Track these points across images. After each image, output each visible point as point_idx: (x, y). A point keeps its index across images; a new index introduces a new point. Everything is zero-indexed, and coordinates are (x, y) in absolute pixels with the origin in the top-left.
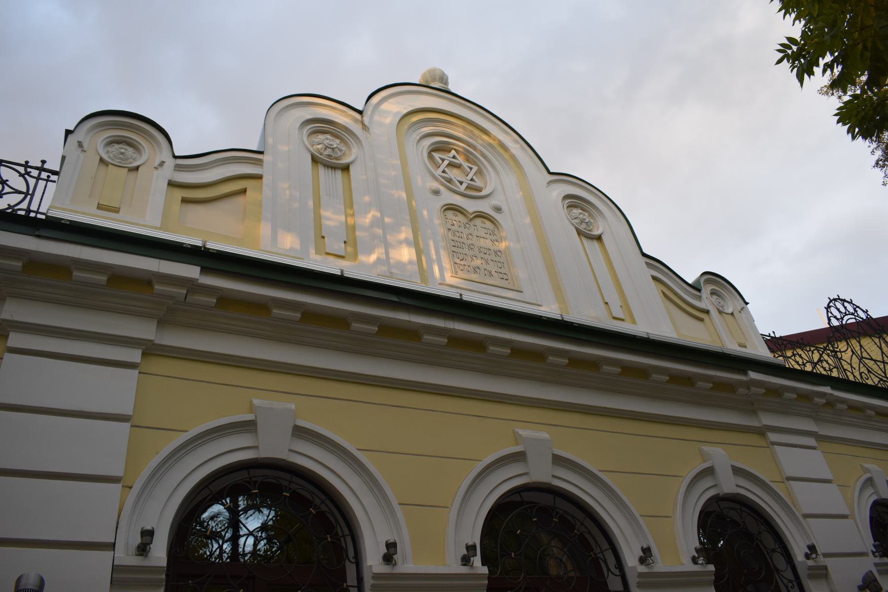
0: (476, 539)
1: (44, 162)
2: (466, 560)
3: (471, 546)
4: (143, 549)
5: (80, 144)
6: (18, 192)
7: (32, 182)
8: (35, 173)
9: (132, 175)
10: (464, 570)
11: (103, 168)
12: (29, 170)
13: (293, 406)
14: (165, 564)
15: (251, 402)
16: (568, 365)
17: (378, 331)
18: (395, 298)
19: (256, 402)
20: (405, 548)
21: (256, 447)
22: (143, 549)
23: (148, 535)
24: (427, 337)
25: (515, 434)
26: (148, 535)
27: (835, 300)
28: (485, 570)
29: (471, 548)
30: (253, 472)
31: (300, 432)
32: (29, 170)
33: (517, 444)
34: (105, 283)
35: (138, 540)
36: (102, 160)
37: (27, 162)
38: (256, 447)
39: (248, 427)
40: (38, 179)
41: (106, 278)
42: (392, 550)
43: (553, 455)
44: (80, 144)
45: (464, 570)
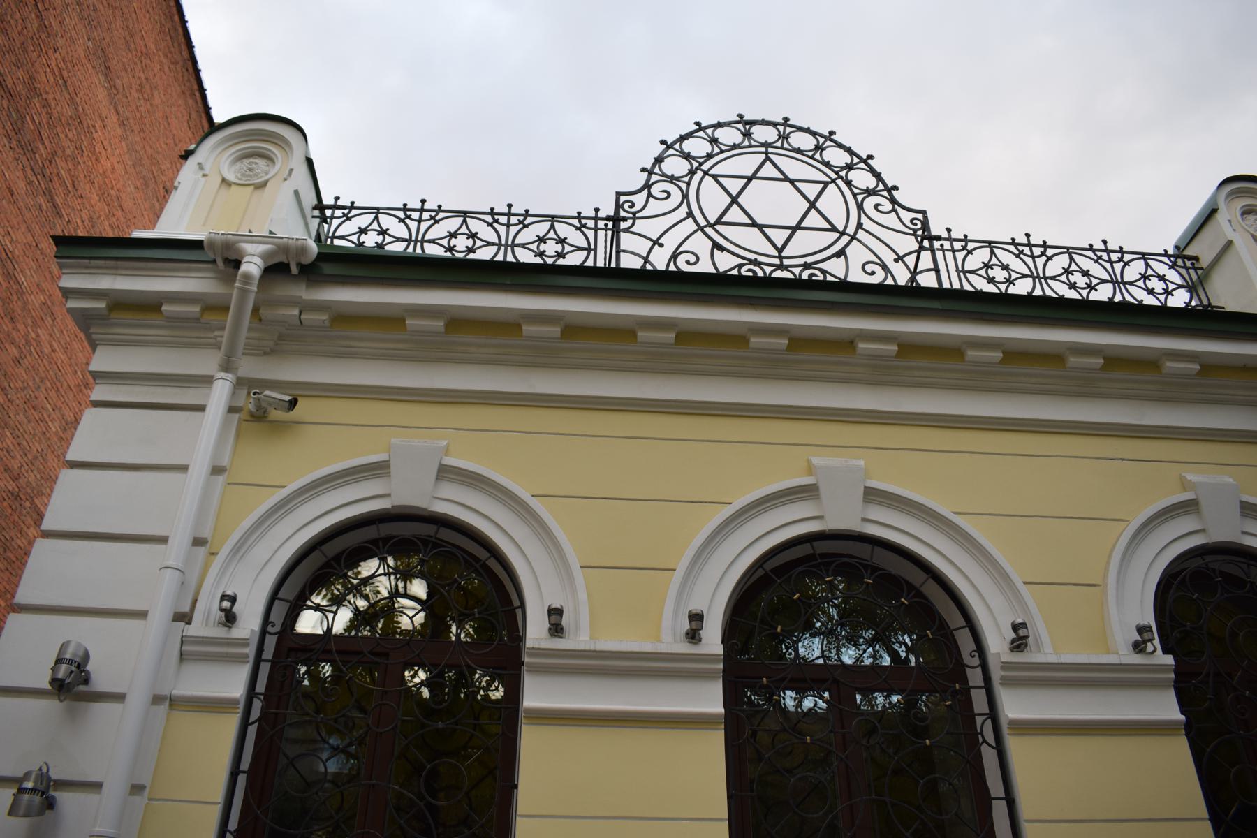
0: (1150, 620)
1: (510, 206)
2: (1138, 647)
3: (556, 609)
4: (693, 636)
5: (201, 166)
6: (579, 249)
7: (590, 234)
8: (503, 219)
9: (258, 192)
10: (1137, 659)
11: (224, 190)
12: (583, 221)
13: (862, 463)
14: (721, 652)
15: (809, 461)
16: (1003, 361)
17: (899, 352)
18: (936, 305)
19: (816, 461)
20: (1040, 629)
21: (1203, 531)
22: (693, 636)
23: (697, 618)
24: (971, 354)
25: (1182, 479)
26: (697, 618)
27: (659, 160)
28: (1169, 660)
29: (1141, 630)
30: (1208, 559)
31: (872, 495)
32: (583, 221)
33: (1185, 490)
34: (673, 341)
35: (686, 626)
36: (224, 180)
37: (405, 205)
38: (1203, 531)
39: (807, 492)
40: (596, 229)
41: (674, 335)
42: (1022, 633)
43: (1241, 502)
44: (201, 166)
45: (1137, 659)
